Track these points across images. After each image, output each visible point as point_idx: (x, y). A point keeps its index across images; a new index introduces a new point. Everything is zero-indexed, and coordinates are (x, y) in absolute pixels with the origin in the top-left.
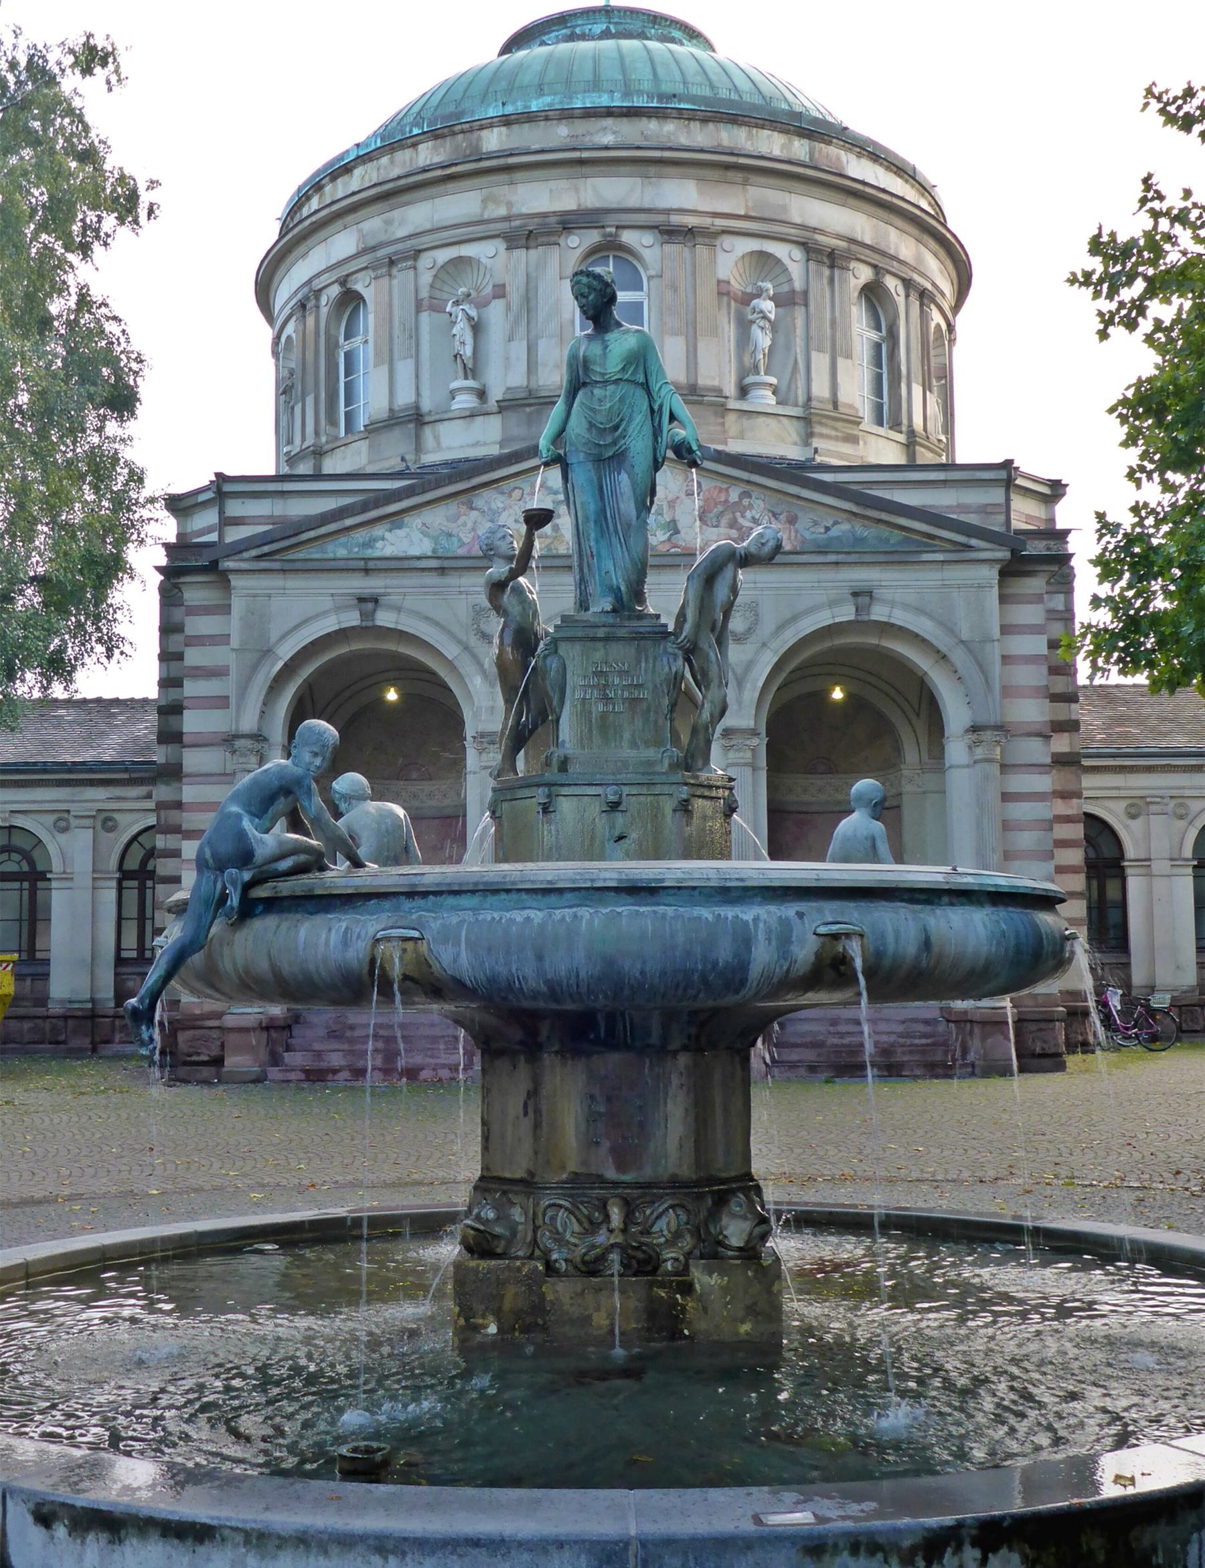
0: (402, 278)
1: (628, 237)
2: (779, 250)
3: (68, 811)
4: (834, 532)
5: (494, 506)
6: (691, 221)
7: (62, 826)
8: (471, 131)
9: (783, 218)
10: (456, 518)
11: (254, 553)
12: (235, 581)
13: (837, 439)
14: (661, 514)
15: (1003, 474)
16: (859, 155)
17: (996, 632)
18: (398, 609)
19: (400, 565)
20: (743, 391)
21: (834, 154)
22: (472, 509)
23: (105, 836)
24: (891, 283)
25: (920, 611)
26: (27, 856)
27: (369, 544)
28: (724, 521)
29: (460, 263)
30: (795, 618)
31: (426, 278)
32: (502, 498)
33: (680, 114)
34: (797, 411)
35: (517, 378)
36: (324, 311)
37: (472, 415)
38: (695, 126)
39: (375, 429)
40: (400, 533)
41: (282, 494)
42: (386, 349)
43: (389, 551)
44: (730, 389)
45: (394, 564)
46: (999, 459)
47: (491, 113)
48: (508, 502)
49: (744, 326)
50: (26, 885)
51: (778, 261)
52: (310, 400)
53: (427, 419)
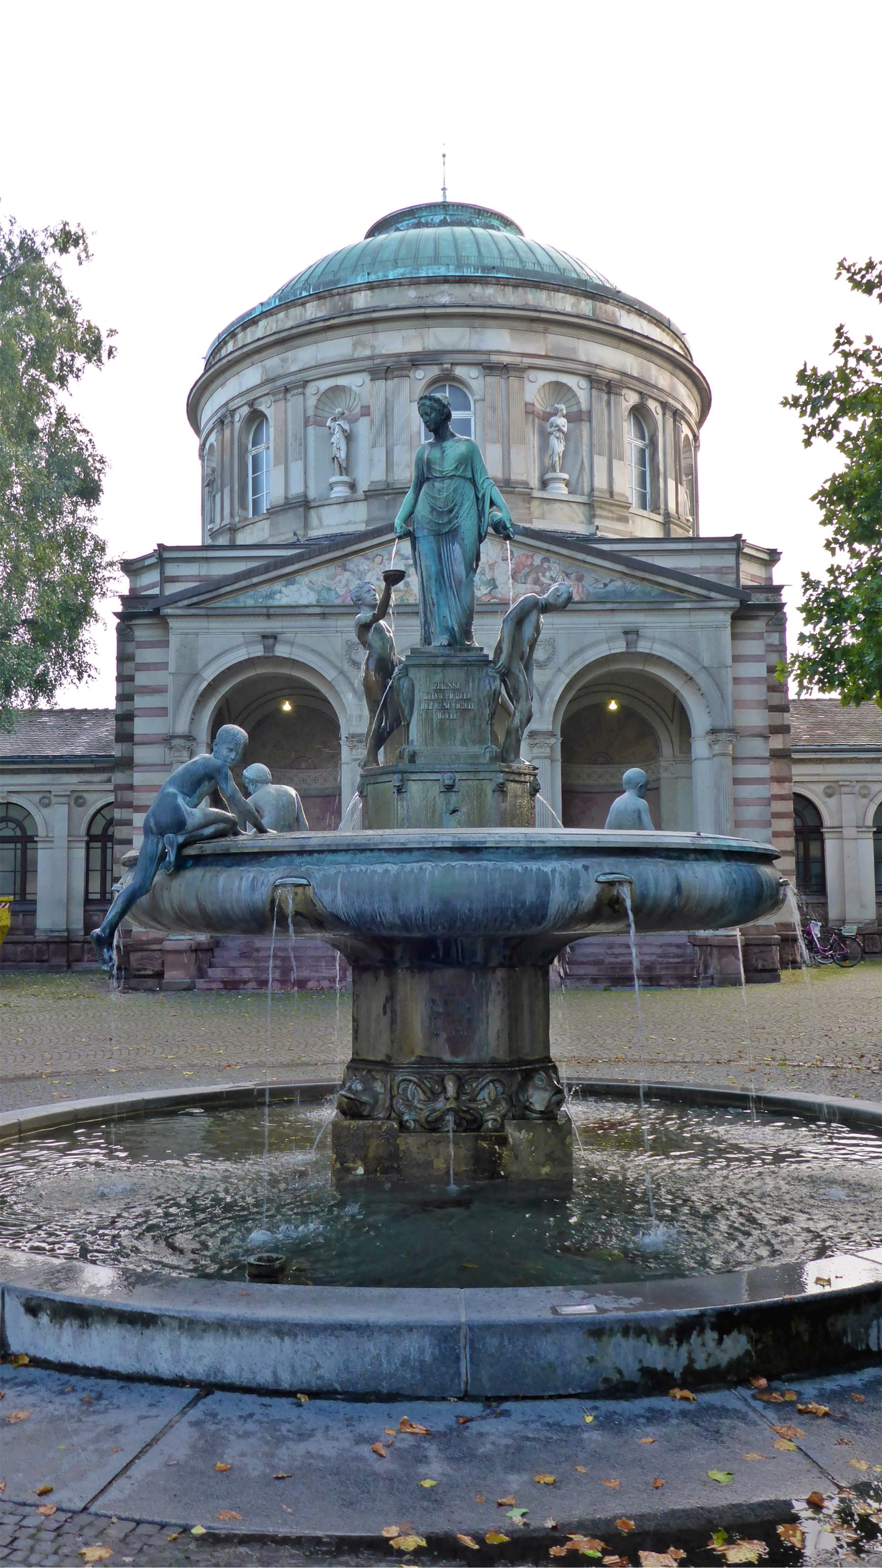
0: (294, 402)
1: (459, 371)
2: (570, 381)
4: (611, 587)
5: (361, 568)
6: (506, 359)
7: (45, 803)
9: (573, 357)
10: (333, 578)
11: (186, 602)
12: (172, 623)
13: (612, 519)
14: (484, 574)
15: (734, 545)
16: (629, 311)
18: (292, 644)
19: (293, 612)
20: (544, 484)
21: (609, 309)
22: (345, 570)
24: (652, 405)
25: (673, 645)
26: (20, 825)
27: (270, 596)
28: (530, 580)
29: (337, 389)
30: (582, 651)
31: (312, 401)
32: (368, 562)
33: (498, 281)
35: (379, 475)
36: (237, 425)
37: (345, 502)
38: (509, 290)
40: (293, 588)
41: (207, 559)
42: (282, 454)
43: (284, 601)
44: (535, 482)
46: (731, 534)
49: (545, 436)
50: (19, 845)
51: (570, 389)
52: (227, 491)
53: (312, 504)
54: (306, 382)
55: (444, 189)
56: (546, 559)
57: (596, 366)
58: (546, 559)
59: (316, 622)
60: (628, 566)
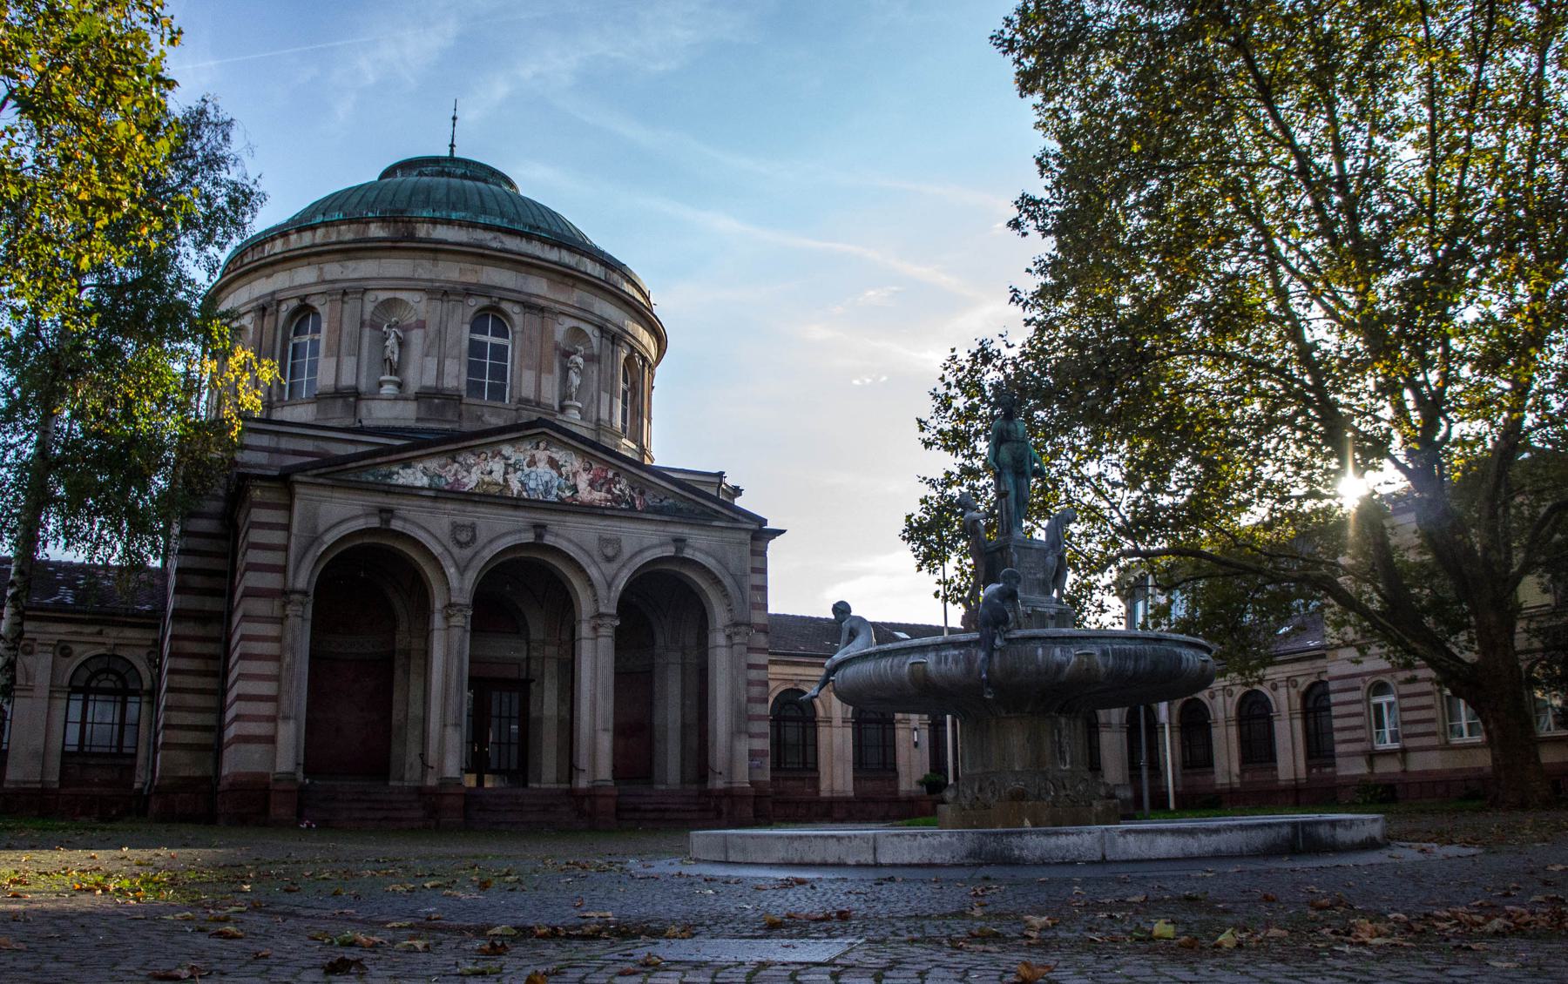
0: (351, 306)
1: (505, 306)
2: (588, 328)
3: (34, 640)
4: (665, 503)
8: (410, 222)
10: (444, 467)
11: (315, 472)
12: (299, 490)
15: (717, 480)
17: (749, 570)
18: (405, 520)
19: (409, 491)
20: (563, 409)
21: (615, 277)
22: (455, 462)
25: (707, 554)
27: (390, 475)
30: (641, 551)
31: (369, 308)
33: (543, 241)
34: (592, 426)
35: (429, 380)
38: (547, 248)
39: (320, 398)
40: (410, 471)
41: (277, 433)
42: (335, 348)
43: (401, 481)
44: (557, 408)
45: (406, 491)
46: (715, 471)
47: (425, 214)
49: (565, 371)
54: (366, 290)
57: (607, 320)
58: (616, 474)
59: (428, 504)
60: (680, 488)
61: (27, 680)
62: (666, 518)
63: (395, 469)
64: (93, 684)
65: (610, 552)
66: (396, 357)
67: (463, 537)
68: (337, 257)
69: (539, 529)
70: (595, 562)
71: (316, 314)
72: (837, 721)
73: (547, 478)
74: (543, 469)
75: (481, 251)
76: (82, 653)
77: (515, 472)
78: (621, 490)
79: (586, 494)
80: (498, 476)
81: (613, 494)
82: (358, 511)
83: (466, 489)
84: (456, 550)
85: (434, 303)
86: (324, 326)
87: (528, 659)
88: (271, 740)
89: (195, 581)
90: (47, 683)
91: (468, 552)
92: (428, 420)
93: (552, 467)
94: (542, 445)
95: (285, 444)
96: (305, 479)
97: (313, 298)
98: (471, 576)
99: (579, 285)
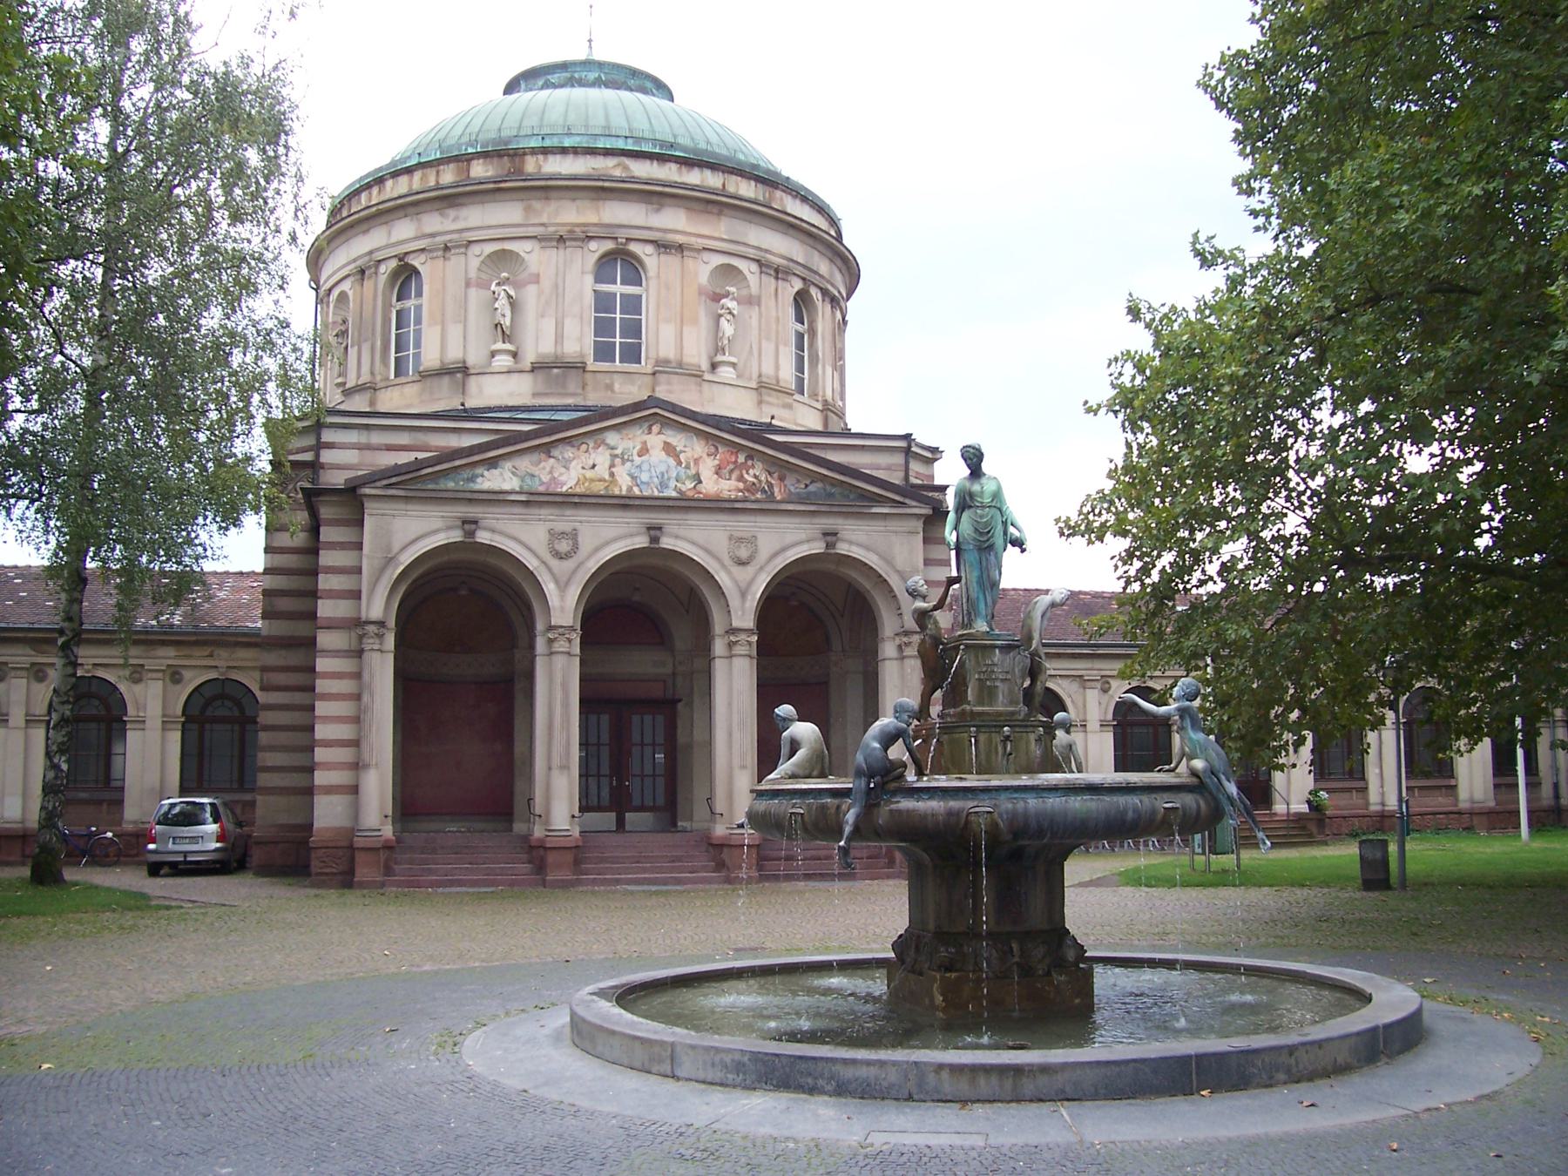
0: (456, 262)
1: (634, 248)
2: (742, 265)
3: (142, 666)
6: (680, 239)
7: (137, 675)
11: (385, 482)
12: (370, 507)
13: (778, 406)
15: (903, 444)
16: (795, 197)
18: (493, 531)
19: (496, 499)
20: (714, 366)
23: (171, 687)
24: (814, 292)
26: (238, 704)
27: (472, 479)
28: (734, 476)
29: (504, 253)
30: (784, 549)
31: (475, 263)
32: (574, 450)
40: (495, 472)
41: (367, 427)
44: (705, 365)
46: (902, 432)
48: (577, 453)
50: (103, 726)
51: (741, 272)
53: (472, 371)
55: (590, 41)
56: (750, 457)
57: (767, 251)
61: (138, 709)
62: (812, 508)
63: (479, 471)
64: (209, 713)
65: (743, 553)
66: (508, 323)
67: (564, 546)
68: (437, 205)
69: (655, 531)
70: (723, 566)
71: (417, 273)
72: (1093, 725)
73: (663, 468)
74: (657, 456)
75: (600, 184)
76: (193, 680)
77: (623, 464)
78: (755, 477)
79: (712, 485)
80: (602, 471)
81: (745, 481)
82: (439, 524)
83: (564, 489)
84: (554, 563)
85: (548, 251)
86: (426, 288)
87: (674, 674)
88: (354, 790)
89: (284, 604)
90: (159, 711)
91: (569, 565)
92: (546, 394)
93: (668, 454)
94: (655, 428)
95: (377, 438)
96: (373, 492)
97: (412, 256)
98: (574, 592)
99: (726, 211)
